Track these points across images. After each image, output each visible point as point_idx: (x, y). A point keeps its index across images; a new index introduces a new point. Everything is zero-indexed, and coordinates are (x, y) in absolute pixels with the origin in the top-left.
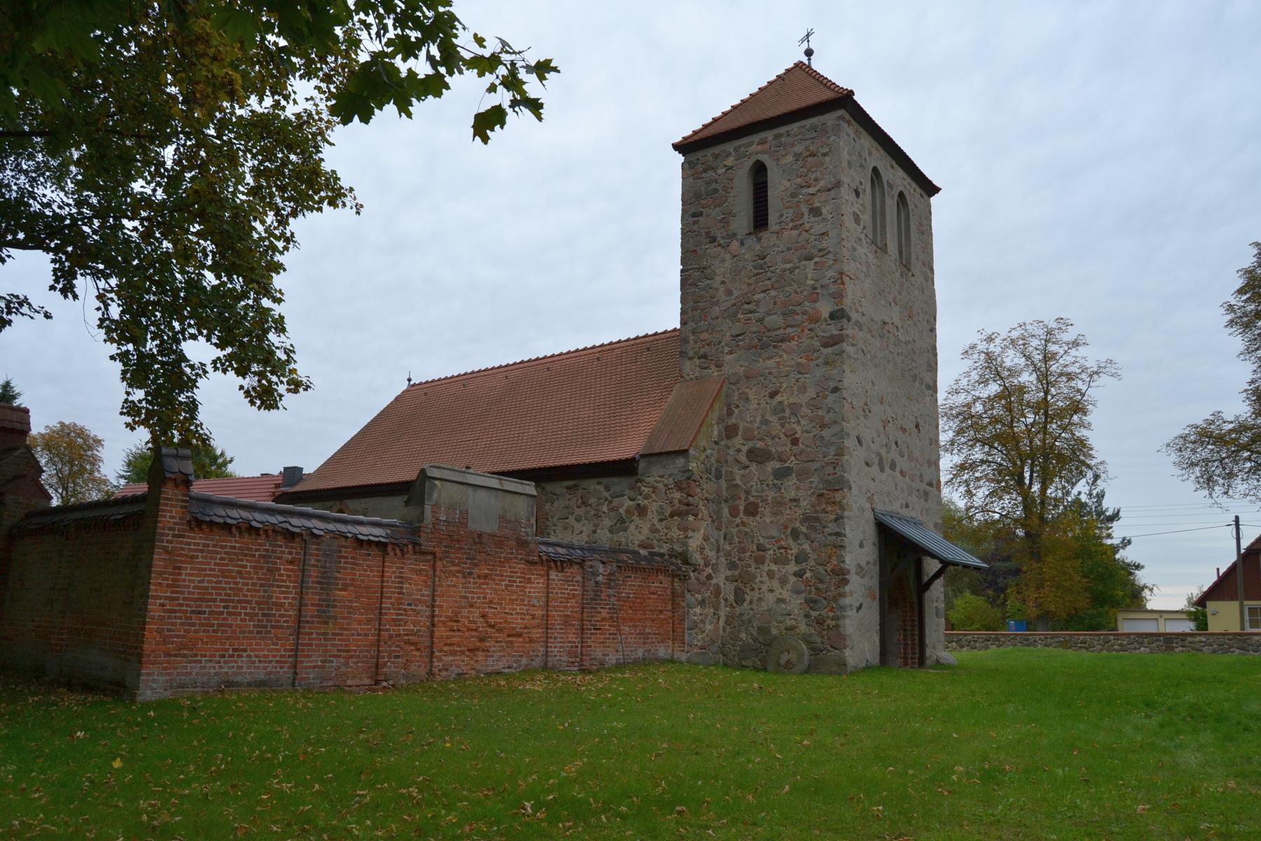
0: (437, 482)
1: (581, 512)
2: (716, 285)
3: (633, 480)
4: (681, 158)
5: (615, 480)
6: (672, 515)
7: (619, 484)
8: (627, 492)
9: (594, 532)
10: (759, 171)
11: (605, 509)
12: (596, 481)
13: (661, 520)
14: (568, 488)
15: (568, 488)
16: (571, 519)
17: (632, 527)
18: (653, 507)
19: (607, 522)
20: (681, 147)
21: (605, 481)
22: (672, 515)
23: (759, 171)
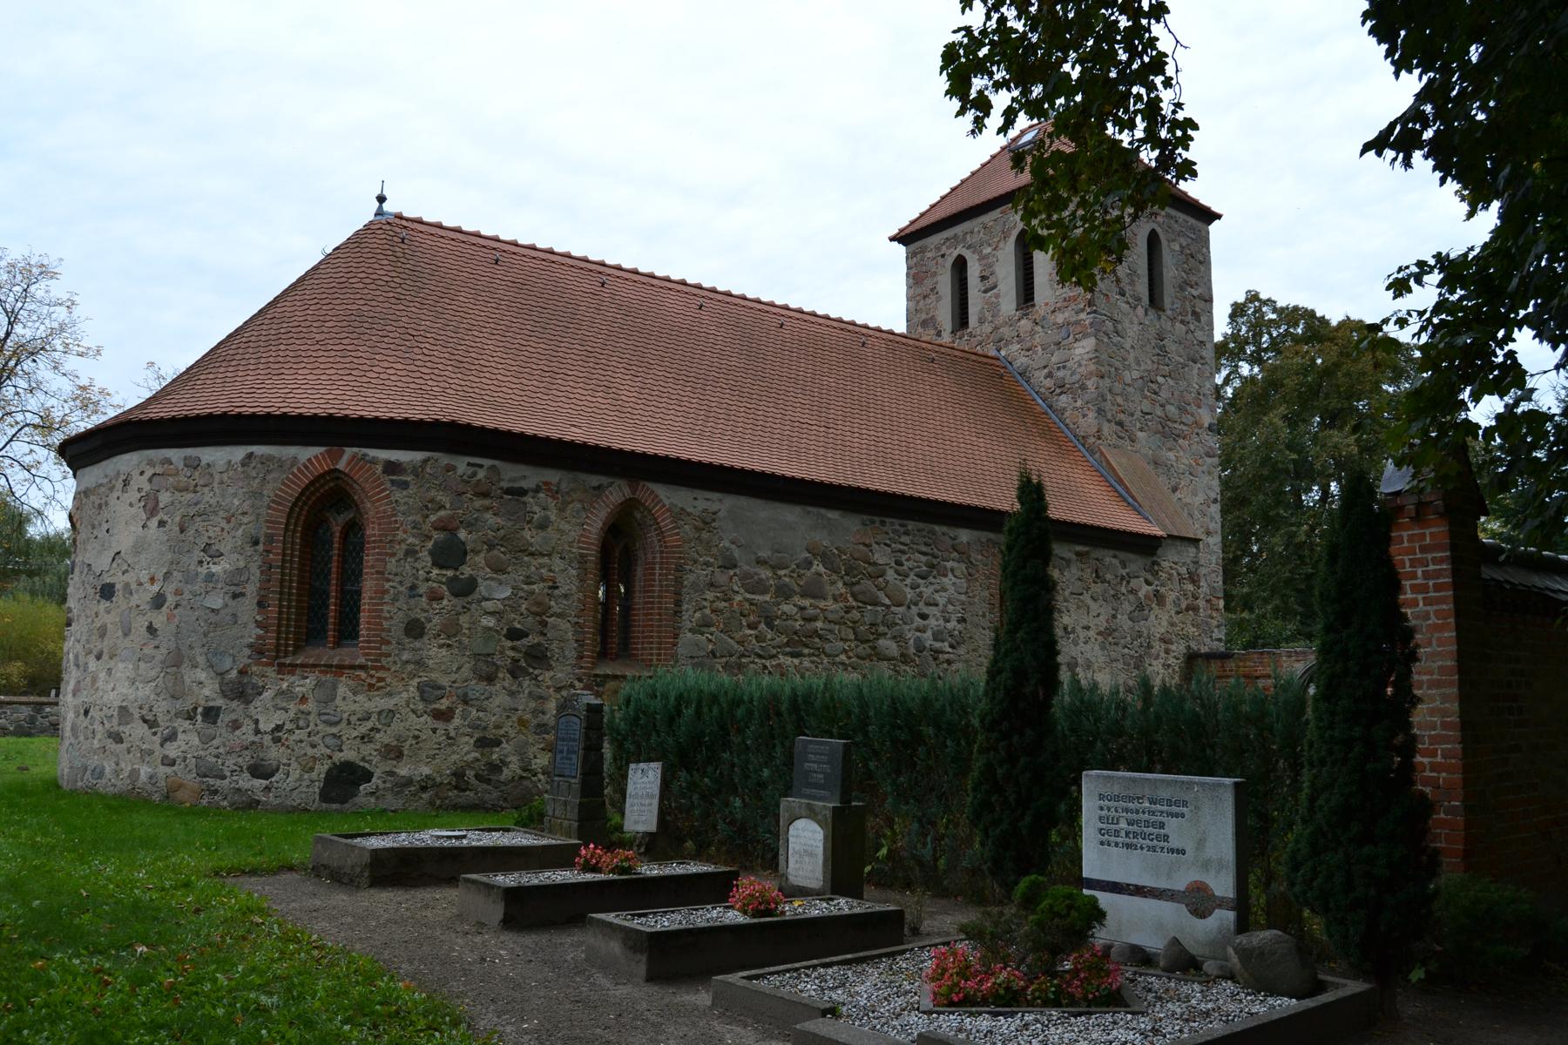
0: (668, 496)
1: (1098, 588)
2: (95, 399)
3: (1148, 561)
4: (901, 250)
5: (1131, 556)
6: (1187, 609)
7: (1136, 563)
8: (1143, 573)
9: (1114, 617)
10: (1153, 241)
11: (1123, 590)
12: (1112, 552)
13: (1178, 613)
14: (1078, 554)
15: (1078, 554)
16: (1086, 597)
17: (1152, 617)
18: (1171, 597)
19: (1127, 607)
20: (903, 238)
21: (1122, 555)
22: (1187, 609)
23: (960, 265)
